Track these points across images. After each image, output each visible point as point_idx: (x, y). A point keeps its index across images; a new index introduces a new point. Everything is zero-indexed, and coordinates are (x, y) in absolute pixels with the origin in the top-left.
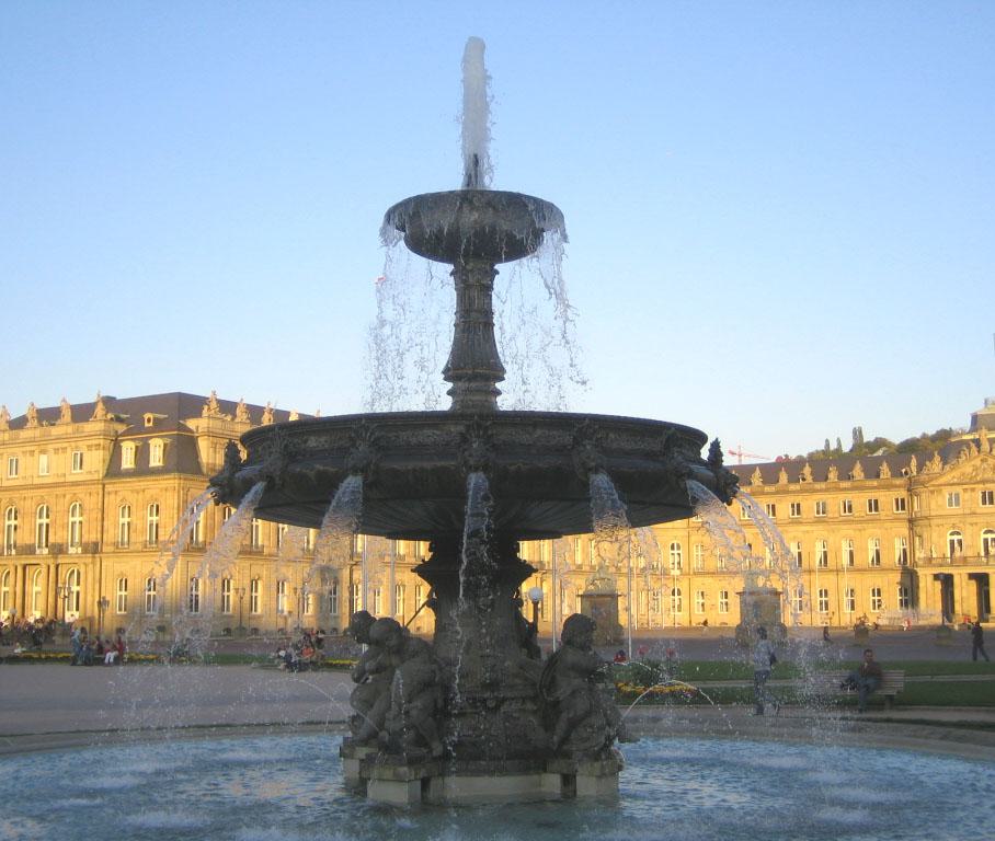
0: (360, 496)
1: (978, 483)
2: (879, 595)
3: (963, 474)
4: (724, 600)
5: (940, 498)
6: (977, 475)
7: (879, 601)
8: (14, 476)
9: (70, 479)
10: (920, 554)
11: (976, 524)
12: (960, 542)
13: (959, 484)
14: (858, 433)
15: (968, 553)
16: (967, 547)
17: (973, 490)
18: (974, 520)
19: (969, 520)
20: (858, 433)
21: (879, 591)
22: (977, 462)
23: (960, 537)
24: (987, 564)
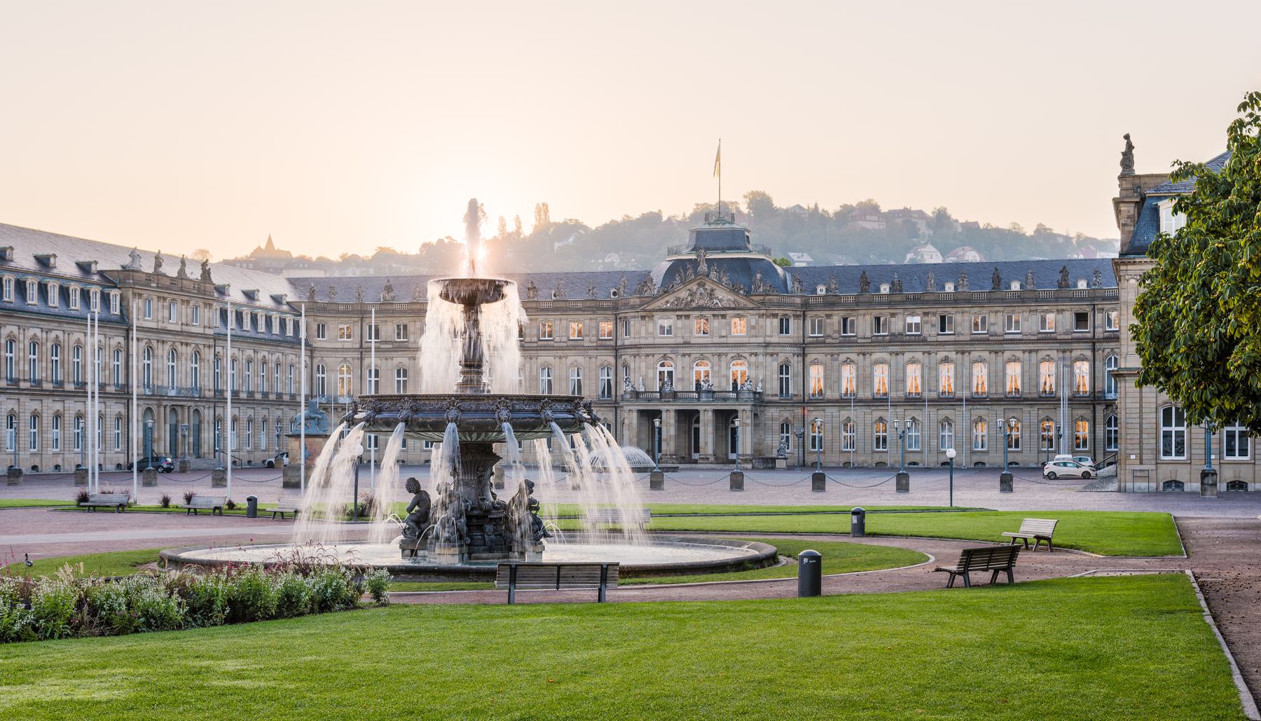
0: (389, 389)
1: (694, 309)
2: (405, 376)
3: (678, 299)
4: (171, 364)
5: (650, 325)
6: (692, 301)
7: (405, 382)
8: (1237, 458)
9: (658, 341)
10: (624, 388)
11: (689, 355)
12: (670, 373)
13: (673, 310)
14: (543, 210)
15: (677, 387)
16: (678, 380)
17: (687, 317)
18: (687, 351)
19: (682, 351)
20: (543, 210)
21: (405, 371)
22: (694, 287)
23: (670, 369)
24: (699, 399)
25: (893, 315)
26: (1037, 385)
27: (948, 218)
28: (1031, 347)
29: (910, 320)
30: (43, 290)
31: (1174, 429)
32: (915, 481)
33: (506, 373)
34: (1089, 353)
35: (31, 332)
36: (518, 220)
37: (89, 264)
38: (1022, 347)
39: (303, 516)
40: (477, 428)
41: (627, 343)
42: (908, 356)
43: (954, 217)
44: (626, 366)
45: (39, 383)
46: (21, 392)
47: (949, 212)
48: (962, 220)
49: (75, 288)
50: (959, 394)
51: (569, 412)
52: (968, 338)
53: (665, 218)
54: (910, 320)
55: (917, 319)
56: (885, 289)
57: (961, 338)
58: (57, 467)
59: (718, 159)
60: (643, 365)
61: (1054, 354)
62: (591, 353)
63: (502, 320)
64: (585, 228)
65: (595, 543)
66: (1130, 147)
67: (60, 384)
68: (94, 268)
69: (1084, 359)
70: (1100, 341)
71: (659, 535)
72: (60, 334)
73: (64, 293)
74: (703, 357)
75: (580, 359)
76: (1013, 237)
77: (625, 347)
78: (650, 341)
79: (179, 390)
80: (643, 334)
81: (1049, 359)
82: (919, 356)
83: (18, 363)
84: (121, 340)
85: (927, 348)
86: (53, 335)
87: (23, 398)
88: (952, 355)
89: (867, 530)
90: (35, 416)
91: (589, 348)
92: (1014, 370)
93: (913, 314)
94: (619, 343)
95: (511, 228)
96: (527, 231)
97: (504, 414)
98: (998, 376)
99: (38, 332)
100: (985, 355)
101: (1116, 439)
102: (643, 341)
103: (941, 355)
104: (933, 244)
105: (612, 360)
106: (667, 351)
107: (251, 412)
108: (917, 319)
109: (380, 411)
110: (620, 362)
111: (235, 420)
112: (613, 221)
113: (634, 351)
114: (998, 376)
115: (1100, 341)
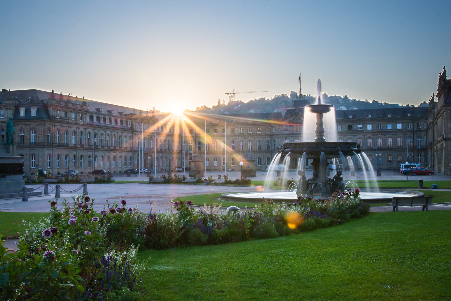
9: (284, 133)
18: (292, 136)
19: (291, 136)
22: (294, 117)
25: (353, 124)
26: (397, 144)
27: (347, 98)
28: (394, 133)
29: (358, 126)
30: (110, 120)
31: (34, 160)
32: (382, 173)
33: (332, 136)
34: (412, 135)
35: (107, 132)
36: (224, 101)
37: (122, 113)
38: (392, 133)
39: (370, 179)
40: (319, 153)
41: (275, 133)
42: (358, 136)
43: (349, 98)
44: (274, 140)
45: (109, 147)
46: (105, 150)
47: (348, 96)
48: (351, 99)
49: (119, 119)
50: (374, 148)
51: (348, 148)
52: (376, 131)
53: (266, 99)
54: (358, 126)
55: (361, 126)
56: (350, 117)
57: (374, 131)
58: (114, 172)
59: (300, 79)
60: (279, 140)
61: (401, 135)
62: (263, 137)
63: (330, 117)
64: (243, 103)
65: (369, 192)
66: (445, 71)
67: (109, 147)
68: (123, 114)
69: (410, 137)
70: (416, 131)
71: (383, 189)
72: (115, 133)
73: (116, 121)
74: (286, 138)
75: (260, 139)
76: (367, 103)
77: (273, 135)
78: (282, 133)
79: (147, 149)
80: (279, 131)
81: (400, 137)
82: (361, 136)
83: (104, 142)
84: (131, 135)
85: (364, 134)
86: (113, 133)
87: (105, 152)
88: (371, 136)
89: (424, 186)
90: (109, 156)
91: (263, 136)
92: (390, 140)
93: (360, 124)
94: (272, 134)
95: (222, 103)
96: (226, 104)
97: (339, 148)
98: (385, 142)
99: (109, 132)
100: (381, 136)
101: (421, 161)
102: (279, 133)
103: (368, 136)
104: (344, 106)
105: (269, 139)
106: (287, 136)
107: (165, 155)
108: (361, 126)
109: (296, 148)
110: (272, 140)
111: (157, 158)
112: (251, 100)
113: (277, 136)
114: (385, 142)
115: (416, 131)
